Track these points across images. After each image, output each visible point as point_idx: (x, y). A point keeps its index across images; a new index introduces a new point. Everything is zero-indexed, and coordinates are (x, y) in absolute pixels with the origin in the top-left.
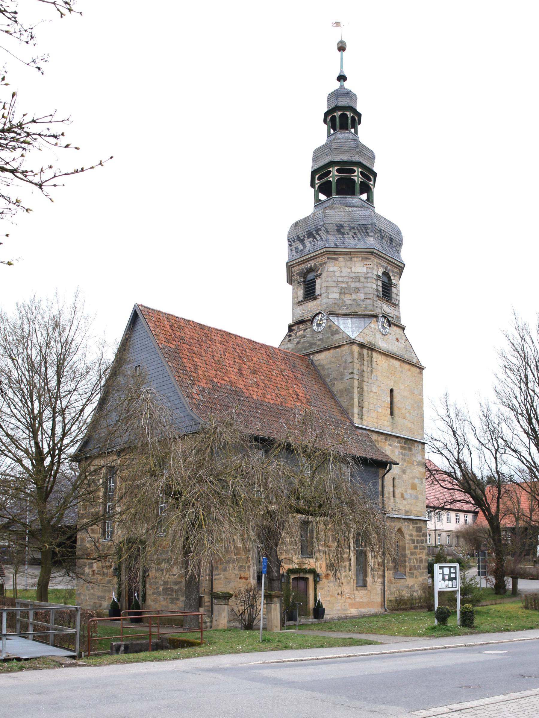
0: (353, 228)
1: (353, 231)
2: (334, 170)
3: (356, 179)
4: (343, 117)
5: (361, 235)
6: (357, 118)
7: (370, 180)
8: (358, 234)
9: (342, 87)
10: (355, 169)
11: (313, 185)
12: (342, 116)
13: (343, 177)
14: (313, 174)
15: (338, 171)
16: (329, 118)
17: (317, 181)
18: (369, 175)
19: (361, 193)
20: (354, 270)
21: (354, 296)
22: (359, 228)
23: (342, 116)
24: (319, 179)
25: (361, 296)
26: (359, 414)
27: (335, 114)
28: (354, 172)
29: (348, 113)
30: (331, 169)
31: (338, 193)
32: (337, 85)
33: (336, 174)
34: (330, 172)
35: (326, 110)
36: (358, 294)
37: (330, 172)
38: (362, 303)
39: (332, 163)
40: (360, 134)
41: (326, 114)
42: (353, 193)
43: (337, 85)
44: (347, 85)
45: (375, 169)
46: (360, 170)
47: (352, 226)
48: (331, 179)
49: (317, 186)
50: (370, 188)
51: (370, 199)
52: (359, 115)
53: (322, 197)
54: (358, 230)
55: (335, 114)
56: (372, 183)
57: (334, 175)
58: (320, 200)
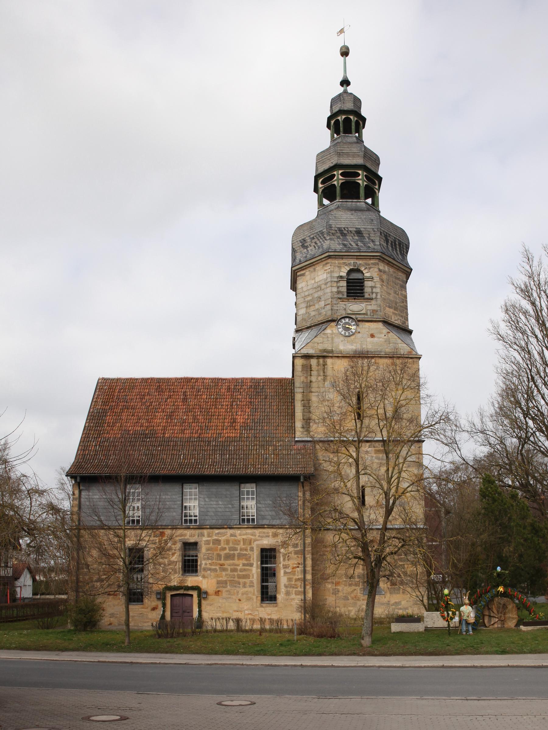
0: (313, 238)
1: (313, 241)
2: (338, 173)
3: (360, 182)
4: (347, 121)
5: (320, 242)
6: (361, 123)
7: (374, 184)
8: (318, 242)
9: (345, 92)
10: (360, 172)
11: (316, 190)
12: (346, 120)
13: (348, 181)
14: (317, 178)
15: (342, 174)
16: (332, 122)
17: (320, 185)
18: (374, 180)
19: (366, 198)
20: (317, 279)
21: (317, 306)
22: (317, 236)
23: (346, 120)
24: (323, 183)
25: (322, 304)
26: (303, 428)
27: (339, 118)
28: (359, 175)
29: (352, 117)
30: (335, 173)
31: (342, 198)
32: (341, 90)
33: (340, 177)
34: (334, 175)
35: (329, 114)
36: (320, 303)
37: (334, 175)
38: (323, 311)
39: (337, 167)
40: (364, 138)
41: (329, 119)
42: (358, 197)
43: (341, 90)
44: (350, 89)
45: (380, 173)
46: (365, 174)
47: (312, 236)
48: (335, 183)
49: (320, 191)
50: (375, 192)
51: (375, 203)
52: (364, 120)
53: (326, 202)
54: (317, 238)
55: (339, 118)
56: (377, 187)
57: (338, 180)
58: (324, 205)
